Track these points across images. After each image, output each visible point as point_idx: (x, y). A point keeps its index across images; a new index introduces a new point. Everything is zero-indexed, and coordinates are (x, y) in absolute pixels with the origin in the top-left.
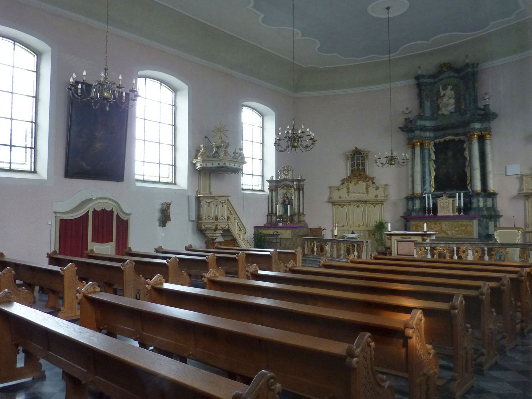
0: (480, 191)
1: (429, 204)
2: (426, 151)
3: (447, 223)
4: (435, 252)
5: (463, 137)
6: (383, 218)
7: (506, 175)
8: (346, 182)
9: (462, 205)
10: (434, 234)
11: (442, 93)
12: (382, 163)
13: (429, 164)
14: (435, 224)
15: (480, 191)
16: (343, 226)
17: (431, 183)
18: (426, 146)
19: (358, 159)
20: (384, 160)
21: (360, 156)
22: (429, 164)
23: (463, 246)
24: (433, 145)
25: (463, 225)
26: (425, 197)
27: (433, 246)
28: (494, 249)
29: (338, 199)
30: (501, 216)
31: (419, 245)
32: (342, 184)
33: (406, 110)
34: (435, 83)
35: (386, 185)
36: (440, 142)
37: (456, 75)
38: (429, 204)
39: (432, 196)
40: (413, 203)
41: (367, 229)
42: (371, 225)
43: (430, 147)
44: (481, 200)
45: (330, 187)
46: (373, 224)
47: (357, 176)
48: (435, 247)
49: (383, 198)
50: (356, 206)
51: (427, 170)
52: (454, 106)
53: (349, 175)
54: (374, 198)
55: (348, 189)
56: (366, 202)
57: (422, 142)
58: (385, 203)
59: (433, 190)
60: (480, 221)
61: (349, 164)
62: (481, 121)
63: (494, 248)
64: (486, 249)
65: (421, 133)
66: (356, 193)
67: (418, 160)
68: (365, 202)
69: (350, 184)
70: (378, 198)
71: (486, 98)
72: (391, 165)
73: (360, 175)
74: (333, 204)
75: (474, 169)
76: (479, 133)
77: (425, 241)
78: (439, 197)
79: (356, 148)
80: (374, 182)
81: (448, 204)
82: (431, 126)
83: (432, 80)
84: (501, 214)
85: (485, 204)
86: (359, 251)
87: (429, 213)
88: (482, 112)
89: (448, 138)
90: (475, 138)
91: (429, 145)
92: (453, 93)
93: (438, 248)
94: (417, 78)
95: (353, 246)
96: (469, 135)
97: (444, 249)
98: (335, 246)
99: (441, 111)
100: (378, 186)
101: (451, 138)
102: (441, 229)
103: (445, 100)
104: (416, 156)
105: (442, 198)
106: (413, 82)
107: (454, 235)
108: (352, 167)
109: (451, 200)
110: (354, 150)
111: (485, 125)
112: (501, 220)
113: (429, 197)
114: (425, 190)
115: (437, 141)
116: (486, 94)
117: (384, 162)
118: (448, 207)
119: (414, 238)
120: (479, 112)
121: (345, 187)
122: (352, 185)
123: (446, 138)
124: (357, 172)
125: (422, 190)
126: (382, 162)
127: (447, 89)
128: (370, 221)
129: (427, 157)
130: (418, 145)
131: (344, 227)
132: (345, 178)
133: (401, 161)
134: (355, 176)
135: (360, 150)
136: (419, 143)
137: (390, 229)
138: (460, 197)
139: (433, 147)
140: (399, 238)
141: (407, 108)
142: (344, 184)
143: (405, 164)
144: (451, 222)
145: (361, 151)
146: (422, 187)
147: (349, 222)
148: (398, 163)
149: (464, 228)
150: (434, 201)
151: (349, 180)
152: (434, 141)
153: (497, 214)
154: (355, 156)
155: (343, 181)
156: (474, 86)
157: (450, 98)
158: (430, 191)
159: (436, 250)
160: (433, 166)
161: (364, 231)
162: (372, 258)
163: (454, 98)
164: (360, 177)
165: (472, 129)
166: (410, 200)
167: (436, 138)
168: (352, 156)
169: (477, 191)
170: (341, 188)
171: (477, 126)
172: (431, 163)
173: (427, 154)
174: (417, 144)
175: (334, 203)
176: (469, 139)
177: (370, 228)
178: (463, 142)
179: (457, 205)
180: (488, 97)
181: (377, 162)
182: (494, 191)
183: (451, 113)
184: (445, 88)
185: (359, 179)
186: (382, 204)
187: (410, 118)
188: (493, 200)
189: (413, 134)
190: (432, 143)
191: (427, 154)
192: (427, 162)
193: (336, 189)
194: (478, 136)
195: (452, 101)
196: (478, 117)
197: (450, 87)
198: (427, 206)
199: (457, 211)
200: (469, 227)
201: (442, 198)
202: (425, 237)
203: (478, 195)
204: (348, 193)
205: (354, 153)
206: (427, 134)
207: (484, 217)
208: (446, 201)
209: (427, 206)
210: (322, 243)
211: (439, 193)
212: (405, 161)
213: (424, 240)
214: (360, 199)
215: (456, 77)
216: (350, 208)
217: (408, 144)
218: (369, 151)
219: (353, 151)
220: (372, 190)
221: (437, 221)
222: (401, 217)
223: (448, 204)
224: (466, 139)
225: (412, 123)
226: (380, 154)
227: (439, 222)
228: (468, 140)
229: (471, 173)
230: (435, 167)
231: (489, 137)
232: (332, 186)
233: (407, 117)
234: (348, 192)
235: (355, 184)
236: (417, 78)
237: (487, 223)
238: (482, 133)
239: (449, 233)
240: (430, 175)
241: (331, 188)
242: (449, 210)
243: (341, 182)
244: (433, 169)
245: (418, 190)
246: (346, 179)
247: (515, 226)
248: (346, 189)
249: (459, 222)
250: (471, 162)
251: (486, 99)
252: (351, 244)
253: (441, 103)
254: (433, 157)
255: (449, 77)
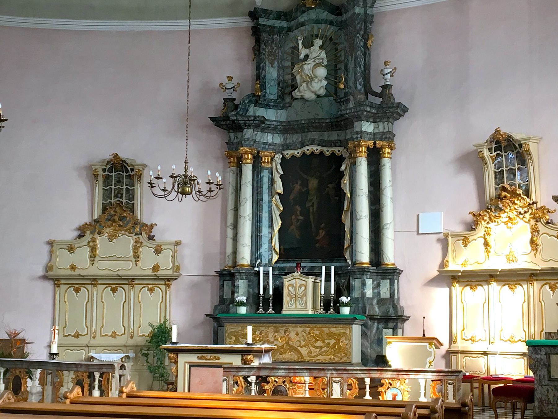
0: (367, 264)
1: (266, 289)
2: (265, 174)
3: (299, 330)
4: (267, 387)
5: (341, 149)
6: (167, 317)
7: (418, 233)
8: (88, 232)
9: (332, 292)
10: (267, 351)
11: (303, 52)
12: (164, 190)
13: (270, 202)
14: (276, 332)
15: (367, 264)
16: (77, 336)
17: (272, 243)
18: (264, 162)
19: (119, 181)
20: (167, 182)
21: (124, 174)
22: (270, 202)
23: (322, 375)
24: (280, 161)
25: (331, 335)
26: (259, 272)
27: (263, 374)
28: (383, 381)
29: (69, 272)
30: (408, 318)
31: (234, 373)
32: (80, 236)
33: (226, 80)
34: (290, 30)
35: (178, 243)
36: (293, 156)
37: (331, 17)
38: (266, 289)
39: (273, 271)
40: (233, 285)
41: (131, 342)
42: (140, 334)
43: (274, 164)
44: (369, 282)
45: (51, 243)
46: (148, 331)
47: (114, 221)
48: (267, 377)
49: (170, 273)
50: (110, 288)
51: (265, 215)
52: (325, 83)
53: (96, 217)
54: (150, 272)
55: (93, 249)
56: (133, 280)
57: (258, 152)
58: (174, 284)
59: (275, 258)
60: (364, 325)
61: (99, 190)
62: (375, 119)
63: (383, 379)
64: (368, 381)
65: (256, 135)
66: (112, 259)
67: (247, 191)
68: (131, 281)
69: (99, 239)
70: (159, 273)
71: (386, 73)
72: (184, 196)
73: (122, 218)
74: (56, 282)
75: (358, 217)
76: (371, 144)
77: (249, 364)
78: (287, 274)
79: (116, 156)
80: (154, 236)
81: (303, 288)
82: (278, 121)
83: (284, 24)
84: (406, 314)
85: (376, 291)
86: (103, 388)
87: (266, 309)
88: (379, 100)
89: (309, 149)
90: (361, 152)
91: (272, 160)
92: (323, 54)
93: (273, 378)
94: (254, 15)
95: (91, 376)
96: (350, 145)
97: (284, 382)
98: (49, 377)
99: (299, 91)
100: (161, 245)
101: (316, 149)
102: (287, 343)
103: (308, 67)
104: (243, 182)
105: (293, 276)
106: (245, 22)
107: (313, 355)
108: (104, 199)
109: (310, 280)
110: (111, 160)
111: (382, 127)
112: (407, 325)
113: (266, 274)
114: (260, 257)
115: (288, 153)
116: (386, 63)
117: (169, 188)
118: (305, 294)
119: (225, 359)
120: (371, 98)
121: (86, 243)
122: (101, 241)
123: (305, 149)
124: (115, 212)
125: (254, 257)
126: (164, 187)
127: (313, 46)
128: (140, 324)
129: (266, 187)
130: (248, 159)
131: (80, 336)
132: (86, 224)
133: (204, 188)
134: (109, 220)
135: (124, 161)
136: (251, 154)
137: (174, 340)
138: (328, 275)
139: (279, 167)
140: (193, 358)
141: (230, 78)
142: (83, 236)
143: (213, 194)
144: (308, 327)
145: (127, 164)
146: (254, 250)
147: (92, 326)
148: (199, 191)
149: (333, 342)
150: (277, 282)
151: (96, 228)
152: (282, 154)
153: (399, 314)
154: (113, 174)
155: (82, 232)
156: (365, 46)
157: (319, 65)
158: (270, 261)
159: (268, 382)
160: (276, 205)
161: (125, 346)
162: (124, 396)
163: (326, 66)
164: (121, 223)
165: (357, 133)
166: (228, 278)
167: (286, 147)
168: (106, 173)
169: (362, 263)
170: (76, 246)
171: (368, 127)
172: (274, 199)
173: (266, 180)
174: (247, 156)
175: (56, 281)
176: (350, 154)
177: (140, 340)
178: (341, 159)
179: (323, 292)
180: (389, 70)
181: (152, 187)
182: (394, 264)
183: (318, 96)
184: (308, 44)
185: (120, 226)
186: (168, 286)
187: (235, 99)
188: (392, 284)
189: (239, 135)
190: (278, 158)
191: (266, 180)
192: (266, 197)
193: (65, 247)
194: (368, 148)
195: (322, 72)
196: (368, 109)
197: (318, 42)
198: (261, 292)
199: (322, 304)
200: (343, 339)
201: (293, 276)
202: (250, 357)
203: (363, 271)
204: (92, 259)
205: (111, 168)
206: (269, 138)
207: (372, 318)
208: (299, 282)
209: (261, 292)
210: (17, 371)
211: (288, 265)
212: (213, 187)
213: (245, 362)
214: (120, 273)
215: (331, 23)
216: (95, 293)
217: (229, 156)
218: (145, 166)
219: (108, 162)
220: (147, 252)
221: (281, 325)
222: (207, 315)
223: (303, 288)
224: (346, 155)
225: (239, 110)
226: (159, 168)
227: (284, 328)
228: (350, 157)
229: (352, 225)
230: (282, 209)
231: (388, 153)
232: (54, 240)
233: (230, 97)
234: (93, 256)
235: (111, 238)
236: (254, 15)
237: (379, 332)
238: (375, 143)
239: (304, 351)
240: (271, 226)
241: (52, 246)
242: (306, 303)
243: (77, 233)
244: (278, 213)
245: (245, 257)
246: (90, 225)
247: (424, 335)
248: (88, 249)
249: (324, 329)
250: (352, 201)
251: (386, 74)
252: (86, 372)
253: (299, 73)
254: (279, 187)
255: (317, 21)
